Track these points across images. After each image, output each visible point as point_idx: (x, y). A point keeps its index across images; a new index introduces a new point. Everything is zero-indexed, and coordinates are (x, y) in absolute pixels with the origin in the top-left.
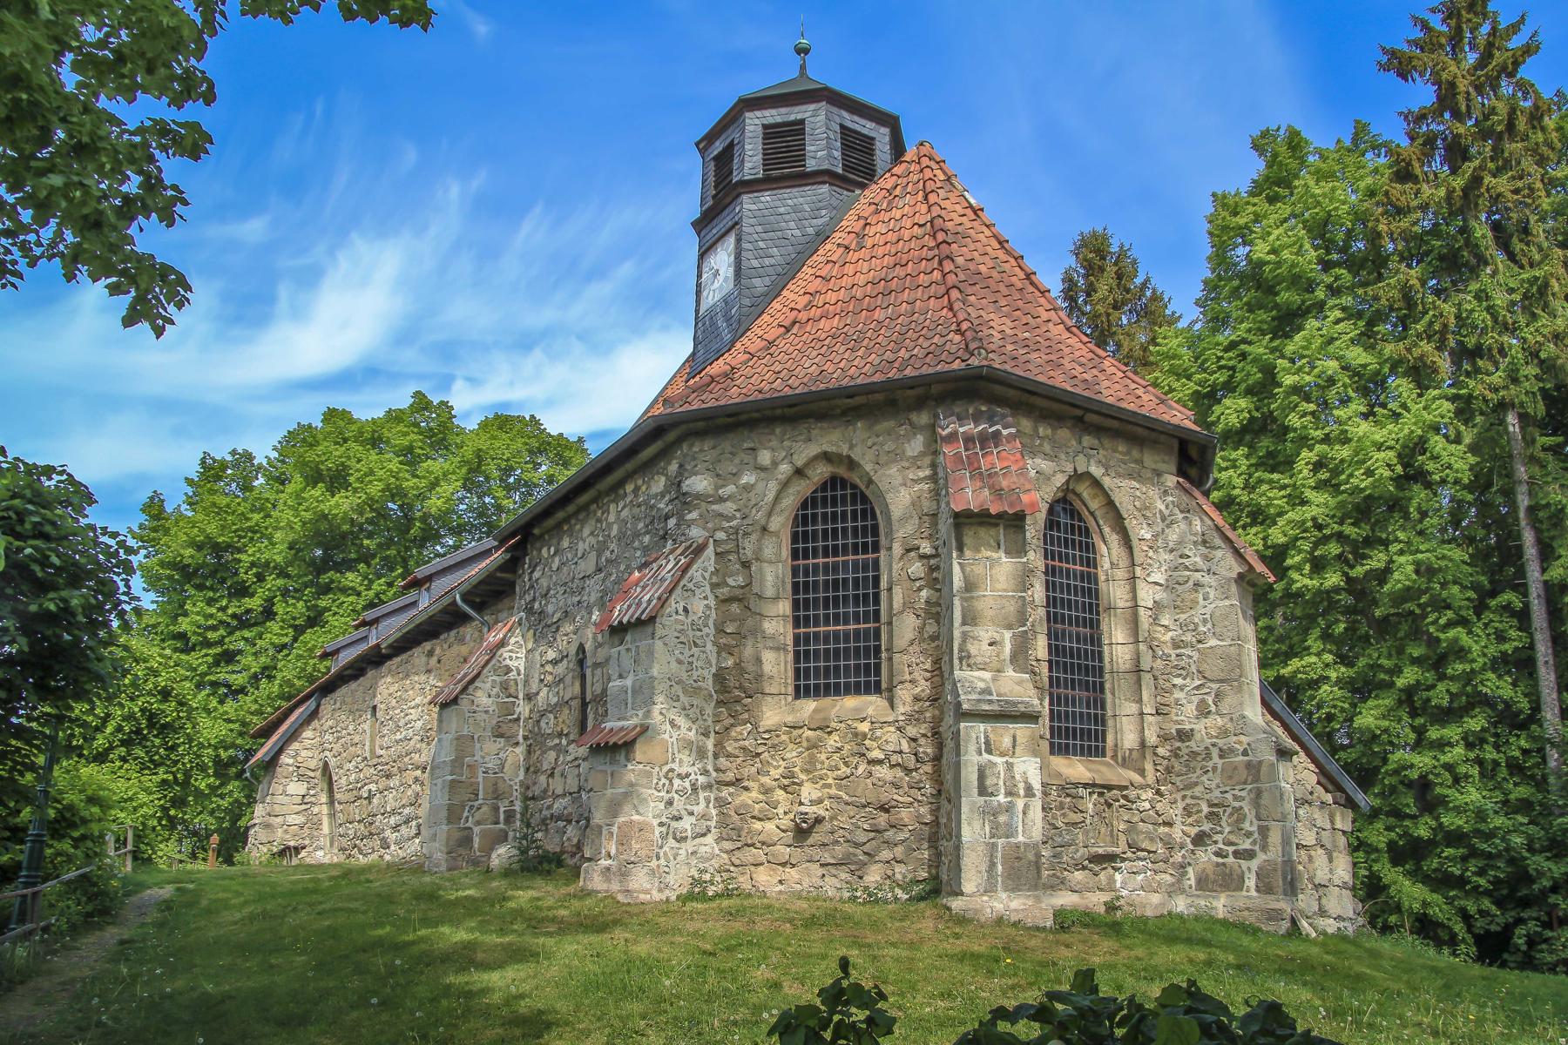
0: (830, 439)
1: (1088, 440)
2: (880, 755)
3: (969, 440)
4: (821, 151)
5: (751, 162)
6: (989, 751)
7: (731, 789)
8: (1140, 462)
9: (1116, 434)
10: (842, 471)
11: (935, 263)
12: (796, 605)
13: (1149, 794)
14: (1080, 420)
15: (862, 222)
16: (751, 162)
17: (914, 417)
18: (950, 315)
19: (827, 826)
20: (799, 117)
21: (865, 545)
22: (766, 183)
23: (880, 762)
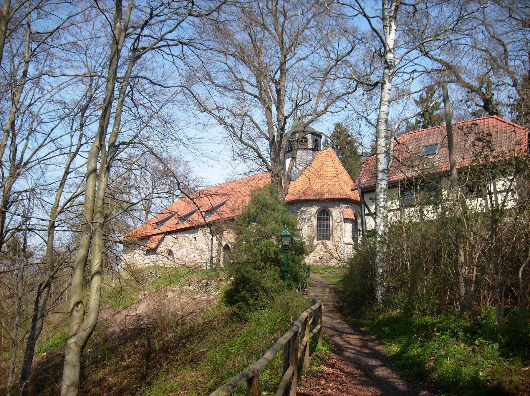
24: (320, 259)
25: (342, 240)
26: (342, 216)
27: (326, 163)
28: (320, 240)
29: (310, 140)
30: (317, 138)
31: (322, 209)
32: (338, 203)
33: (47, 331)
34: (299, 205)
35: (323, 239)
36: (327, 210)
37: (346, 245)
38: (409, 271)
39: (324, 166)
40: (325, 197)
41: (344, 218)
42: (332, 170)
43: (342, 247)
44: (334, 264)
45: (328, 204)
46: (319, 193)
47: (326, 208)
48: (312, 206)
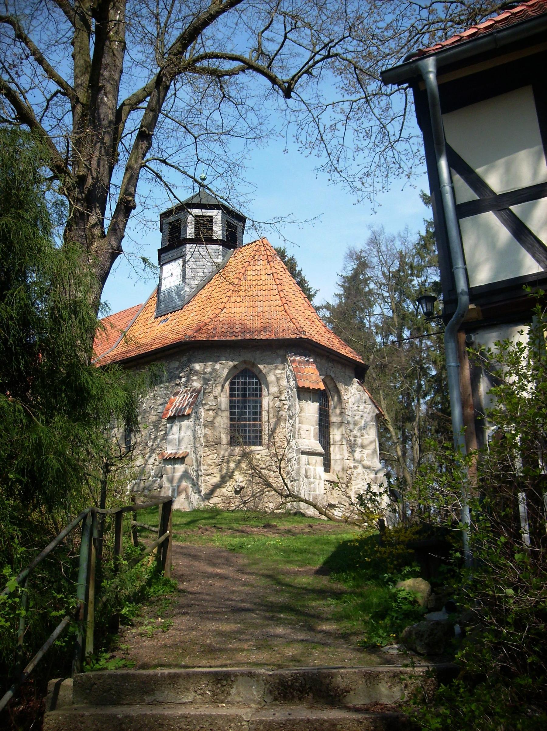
0: (247, 356)
1: (330, 364)
2: (264, 466)
3: (300, 362)
4: (218, 231)
5: (190, 231)
6: (309, 464)
7: (209, 477)
8: (345, 372)
9: (338, 362)
10: (249, 367)
11: (277, 293)
12: (231, 413)
13: (344, 486)
14: (328, 357)
15: (244, 269)
16: (190, 231)
17: (278, 351)
18: (286, 314)
19: (245, 490)
20: (210, 214)
21: (257, 394)
22: (196, 241)
23: (264, 469)
24: (237, 492)
25: (293, 443)
26: (292, 383)
27: (254, 268)
28: (238, 444)
29: (220, 224)
30: (235, 222)
31: (243, 366)
32: (281, 352)
33: (247, 713)
34: (184, 359)
35: (246, 444)
36: (254, 370)
37: (304, 458)
38: (211, 544)
39: (249, 273)
40: (263, 336)
41: (298, 388)
42: (269, 282)
43: (293, 462)
44: (271, 505)
45: (258, 354)
46: (245, 330)
47: (254, 365)
48: (216, 360)
